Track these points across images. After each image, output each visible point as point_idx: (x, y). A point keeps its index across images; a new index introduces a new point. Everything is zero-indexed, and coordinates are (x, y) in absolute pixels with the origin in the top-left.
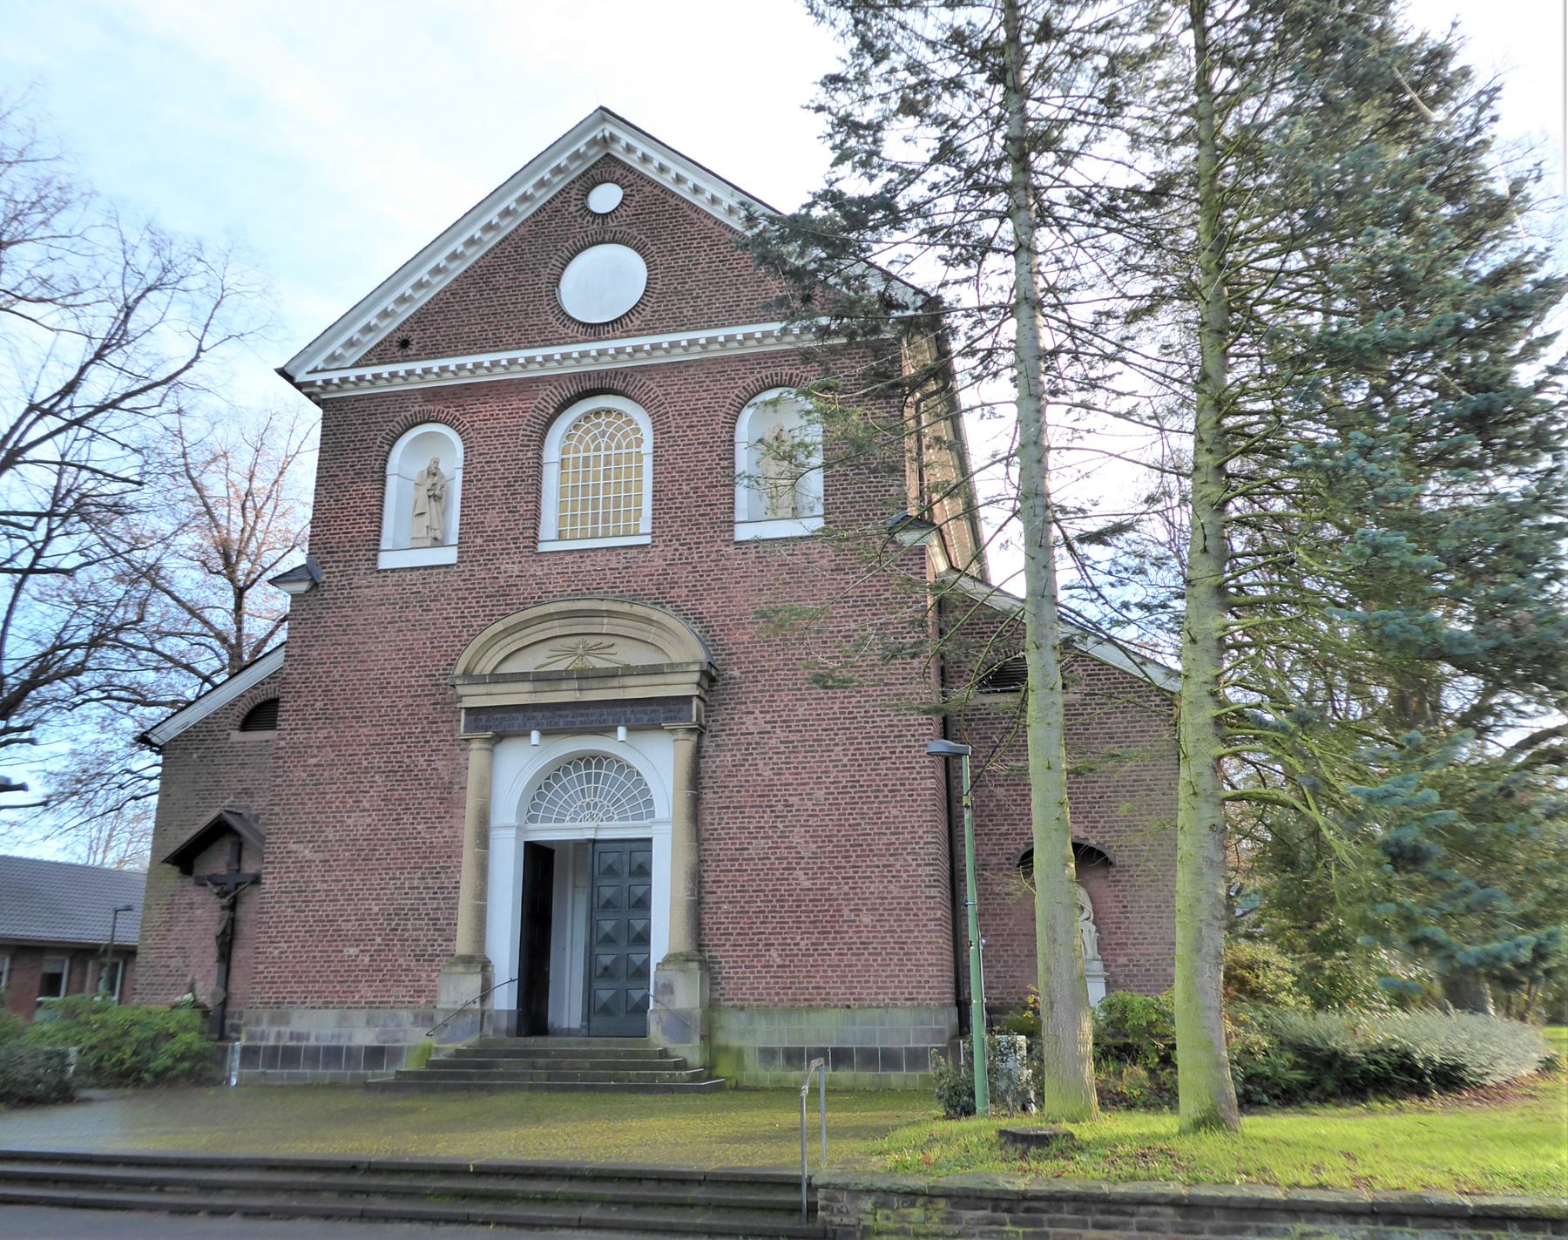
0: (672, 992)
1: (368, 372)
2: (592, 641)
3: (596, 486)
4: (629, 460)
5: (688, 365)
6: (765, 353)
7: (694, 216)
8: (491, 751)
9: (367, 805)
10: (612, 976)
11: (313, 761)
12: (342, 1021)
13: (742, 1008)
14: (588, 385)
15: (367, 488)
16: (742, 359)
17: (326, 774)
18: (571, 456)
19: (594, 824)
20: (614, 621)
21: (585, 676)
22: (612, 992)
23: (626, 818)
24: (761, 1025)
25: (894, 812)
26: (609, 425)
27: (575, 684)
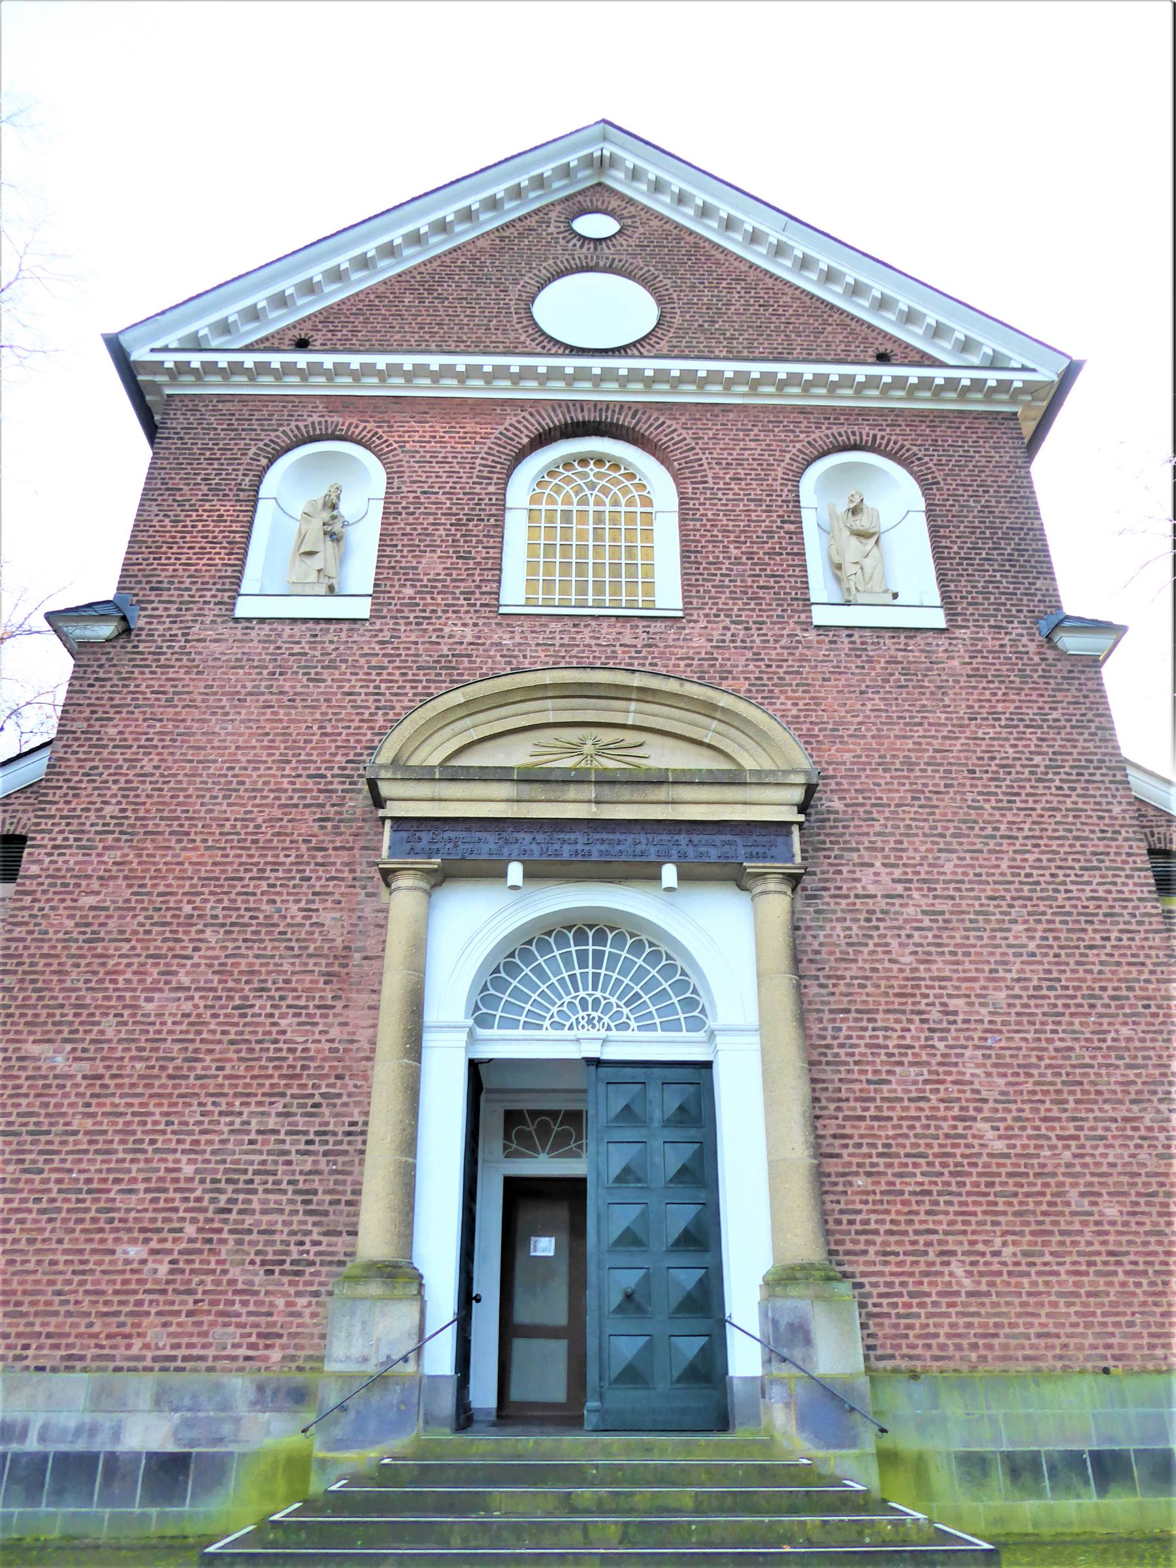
0: (808, 1341)
5: (726, 408)
6: (834, 408)
8: (430, 895)
9: (186, 981)
10: (640, 1310)
11: (91, 900)
12: (99, 1398)
13: (914, 1375)
15: (227, 509)
17: (112, 925)
18: (544, 507)
19: (603, 1033)
21: (606, 780)
23: (652, 1027)
24: (954, 1407)
25: (1125, 1031)
26: (598, 475)
27: (591, 792)
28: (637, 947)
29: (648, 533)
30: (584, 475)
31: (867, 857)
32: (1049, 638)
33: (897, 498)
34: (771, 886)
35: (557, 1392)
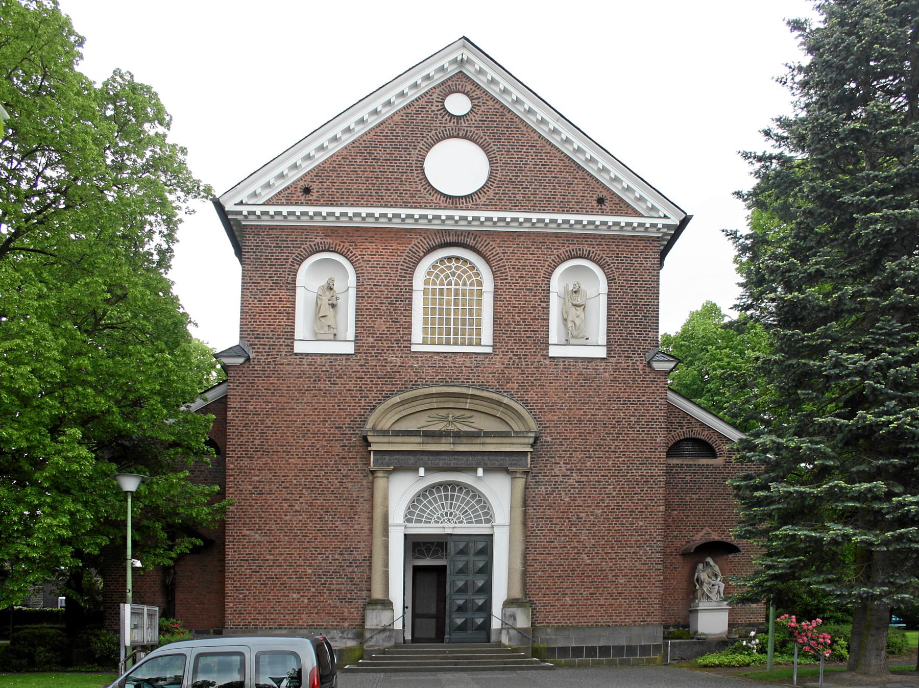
1: (272, 210)
2: (458, 413)
3: (449, 310)
4: (472, 294)
5: (520, 234)
7: (524, 129)
9: (298, 509)
11: (257, 478)
14: (448, 239)
16: (557, 235)
17: (267, 487)
19: (454, 525)
20: (474, 401)
21: (458, 435)
22: (463, 620)
23: (472, 522)
25: (641, 523)
26: (457, 268)
28: (467, 493)
29: (479, 303)
30: (450, 268)
31: (558, 460)
32: (649, 363)
33: (596, 286)
34: (518, 476)
35: (238, 658)
